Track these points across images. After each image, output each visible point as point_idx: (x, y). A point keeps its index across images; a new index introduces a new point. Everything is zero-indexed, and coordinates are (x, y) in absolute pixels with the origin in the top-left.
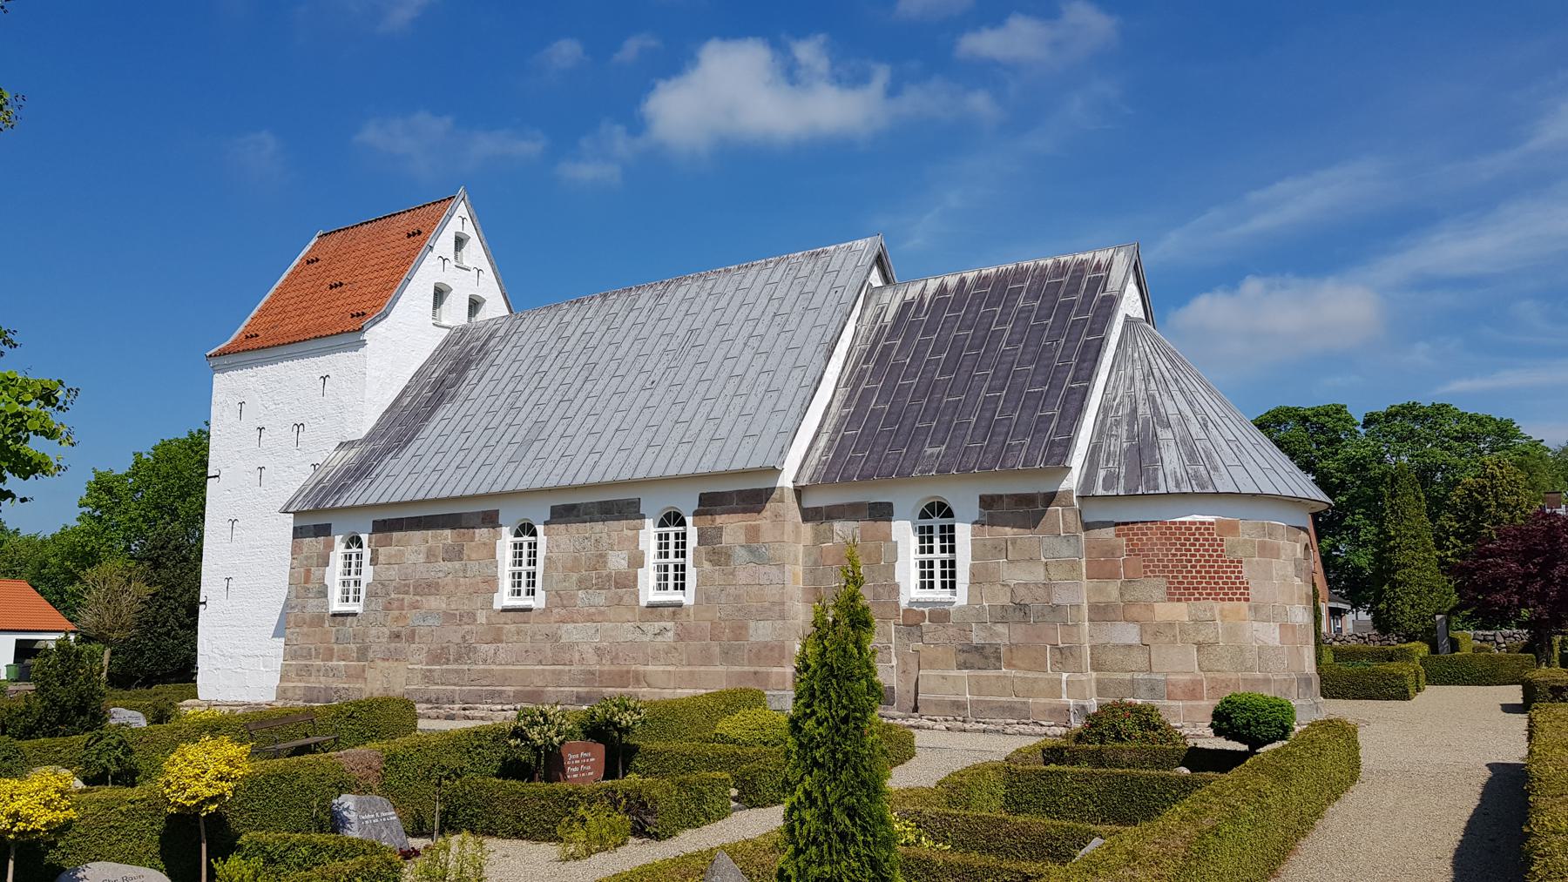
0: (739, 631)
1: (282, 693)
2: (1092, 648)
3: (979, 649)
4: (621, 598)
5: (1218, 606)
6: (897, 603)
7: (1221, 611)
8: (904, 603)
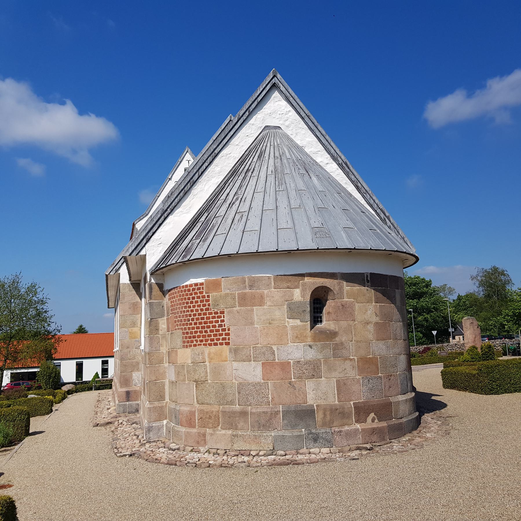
5: (207, 350)
7: (209, 354)
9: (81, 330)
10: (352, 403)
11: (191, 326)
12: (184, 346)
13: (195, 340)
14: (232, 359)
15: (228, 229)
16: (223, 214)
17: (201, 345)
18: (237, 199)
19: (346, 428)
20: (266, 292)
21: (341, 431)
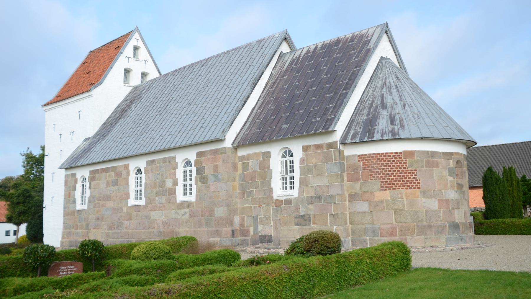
0: (211, 212)
1: (62, 243)
2: (350, 214)
3: (303, 216)
4: (170, 200)
5: (404, 192)
6: (272, 197)
7: (406, 194)
8: (275, 197)
12: (381, 190)
20: (439, 160)
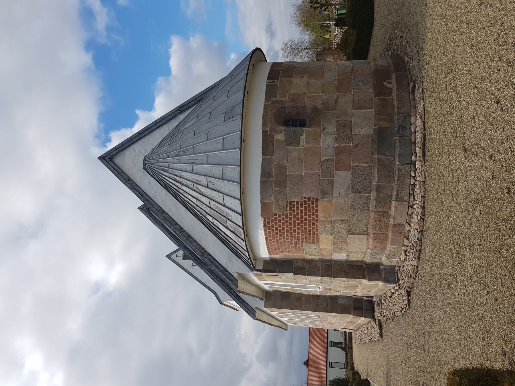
9: (306, 363)
10: (374, 98)
11: (300, 233)
13: (313, 230)
14: (331, 196)
15: (220, 194)
16: (207, 200)
17: (317, 225)
18: (197, 188)
19: (395, 103)
20: (275, 163)
21: (398, 107)
